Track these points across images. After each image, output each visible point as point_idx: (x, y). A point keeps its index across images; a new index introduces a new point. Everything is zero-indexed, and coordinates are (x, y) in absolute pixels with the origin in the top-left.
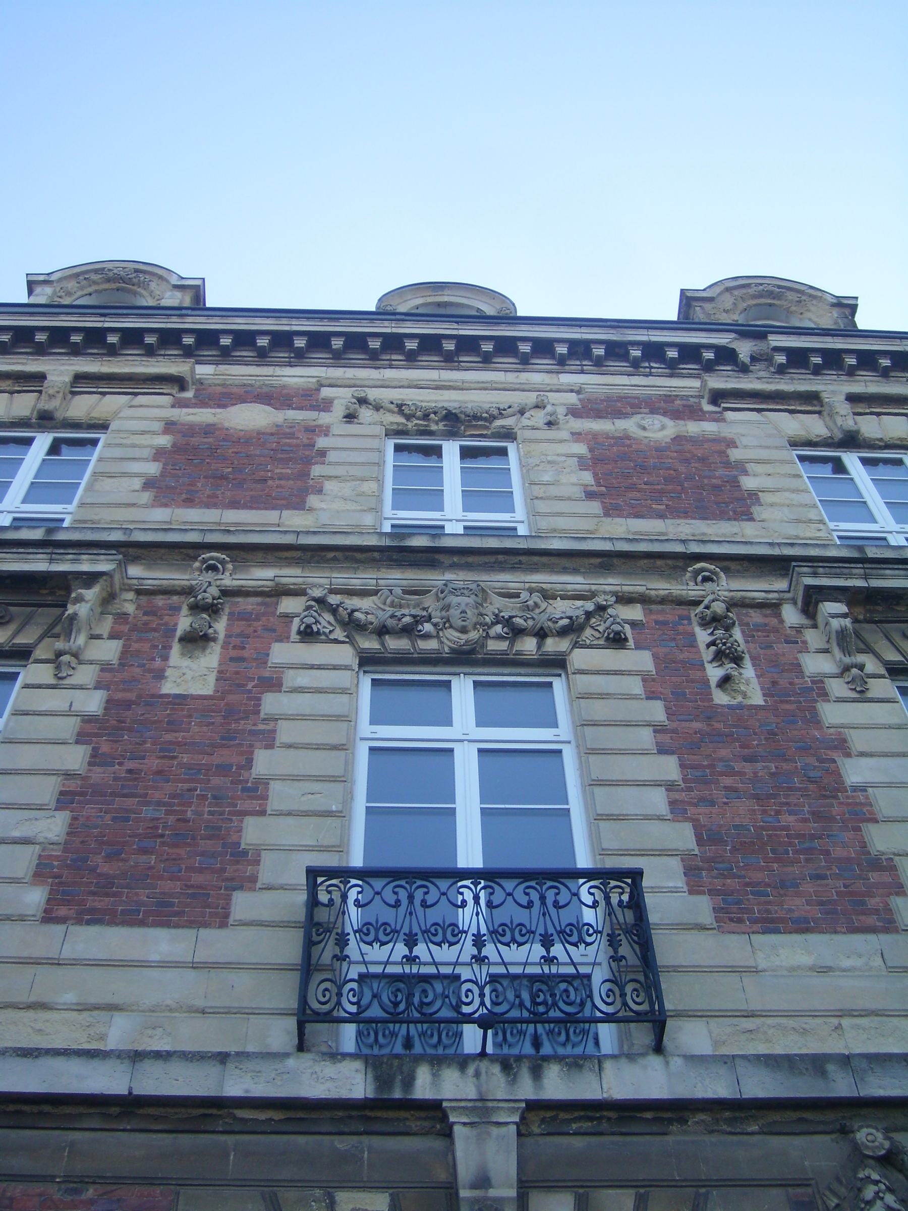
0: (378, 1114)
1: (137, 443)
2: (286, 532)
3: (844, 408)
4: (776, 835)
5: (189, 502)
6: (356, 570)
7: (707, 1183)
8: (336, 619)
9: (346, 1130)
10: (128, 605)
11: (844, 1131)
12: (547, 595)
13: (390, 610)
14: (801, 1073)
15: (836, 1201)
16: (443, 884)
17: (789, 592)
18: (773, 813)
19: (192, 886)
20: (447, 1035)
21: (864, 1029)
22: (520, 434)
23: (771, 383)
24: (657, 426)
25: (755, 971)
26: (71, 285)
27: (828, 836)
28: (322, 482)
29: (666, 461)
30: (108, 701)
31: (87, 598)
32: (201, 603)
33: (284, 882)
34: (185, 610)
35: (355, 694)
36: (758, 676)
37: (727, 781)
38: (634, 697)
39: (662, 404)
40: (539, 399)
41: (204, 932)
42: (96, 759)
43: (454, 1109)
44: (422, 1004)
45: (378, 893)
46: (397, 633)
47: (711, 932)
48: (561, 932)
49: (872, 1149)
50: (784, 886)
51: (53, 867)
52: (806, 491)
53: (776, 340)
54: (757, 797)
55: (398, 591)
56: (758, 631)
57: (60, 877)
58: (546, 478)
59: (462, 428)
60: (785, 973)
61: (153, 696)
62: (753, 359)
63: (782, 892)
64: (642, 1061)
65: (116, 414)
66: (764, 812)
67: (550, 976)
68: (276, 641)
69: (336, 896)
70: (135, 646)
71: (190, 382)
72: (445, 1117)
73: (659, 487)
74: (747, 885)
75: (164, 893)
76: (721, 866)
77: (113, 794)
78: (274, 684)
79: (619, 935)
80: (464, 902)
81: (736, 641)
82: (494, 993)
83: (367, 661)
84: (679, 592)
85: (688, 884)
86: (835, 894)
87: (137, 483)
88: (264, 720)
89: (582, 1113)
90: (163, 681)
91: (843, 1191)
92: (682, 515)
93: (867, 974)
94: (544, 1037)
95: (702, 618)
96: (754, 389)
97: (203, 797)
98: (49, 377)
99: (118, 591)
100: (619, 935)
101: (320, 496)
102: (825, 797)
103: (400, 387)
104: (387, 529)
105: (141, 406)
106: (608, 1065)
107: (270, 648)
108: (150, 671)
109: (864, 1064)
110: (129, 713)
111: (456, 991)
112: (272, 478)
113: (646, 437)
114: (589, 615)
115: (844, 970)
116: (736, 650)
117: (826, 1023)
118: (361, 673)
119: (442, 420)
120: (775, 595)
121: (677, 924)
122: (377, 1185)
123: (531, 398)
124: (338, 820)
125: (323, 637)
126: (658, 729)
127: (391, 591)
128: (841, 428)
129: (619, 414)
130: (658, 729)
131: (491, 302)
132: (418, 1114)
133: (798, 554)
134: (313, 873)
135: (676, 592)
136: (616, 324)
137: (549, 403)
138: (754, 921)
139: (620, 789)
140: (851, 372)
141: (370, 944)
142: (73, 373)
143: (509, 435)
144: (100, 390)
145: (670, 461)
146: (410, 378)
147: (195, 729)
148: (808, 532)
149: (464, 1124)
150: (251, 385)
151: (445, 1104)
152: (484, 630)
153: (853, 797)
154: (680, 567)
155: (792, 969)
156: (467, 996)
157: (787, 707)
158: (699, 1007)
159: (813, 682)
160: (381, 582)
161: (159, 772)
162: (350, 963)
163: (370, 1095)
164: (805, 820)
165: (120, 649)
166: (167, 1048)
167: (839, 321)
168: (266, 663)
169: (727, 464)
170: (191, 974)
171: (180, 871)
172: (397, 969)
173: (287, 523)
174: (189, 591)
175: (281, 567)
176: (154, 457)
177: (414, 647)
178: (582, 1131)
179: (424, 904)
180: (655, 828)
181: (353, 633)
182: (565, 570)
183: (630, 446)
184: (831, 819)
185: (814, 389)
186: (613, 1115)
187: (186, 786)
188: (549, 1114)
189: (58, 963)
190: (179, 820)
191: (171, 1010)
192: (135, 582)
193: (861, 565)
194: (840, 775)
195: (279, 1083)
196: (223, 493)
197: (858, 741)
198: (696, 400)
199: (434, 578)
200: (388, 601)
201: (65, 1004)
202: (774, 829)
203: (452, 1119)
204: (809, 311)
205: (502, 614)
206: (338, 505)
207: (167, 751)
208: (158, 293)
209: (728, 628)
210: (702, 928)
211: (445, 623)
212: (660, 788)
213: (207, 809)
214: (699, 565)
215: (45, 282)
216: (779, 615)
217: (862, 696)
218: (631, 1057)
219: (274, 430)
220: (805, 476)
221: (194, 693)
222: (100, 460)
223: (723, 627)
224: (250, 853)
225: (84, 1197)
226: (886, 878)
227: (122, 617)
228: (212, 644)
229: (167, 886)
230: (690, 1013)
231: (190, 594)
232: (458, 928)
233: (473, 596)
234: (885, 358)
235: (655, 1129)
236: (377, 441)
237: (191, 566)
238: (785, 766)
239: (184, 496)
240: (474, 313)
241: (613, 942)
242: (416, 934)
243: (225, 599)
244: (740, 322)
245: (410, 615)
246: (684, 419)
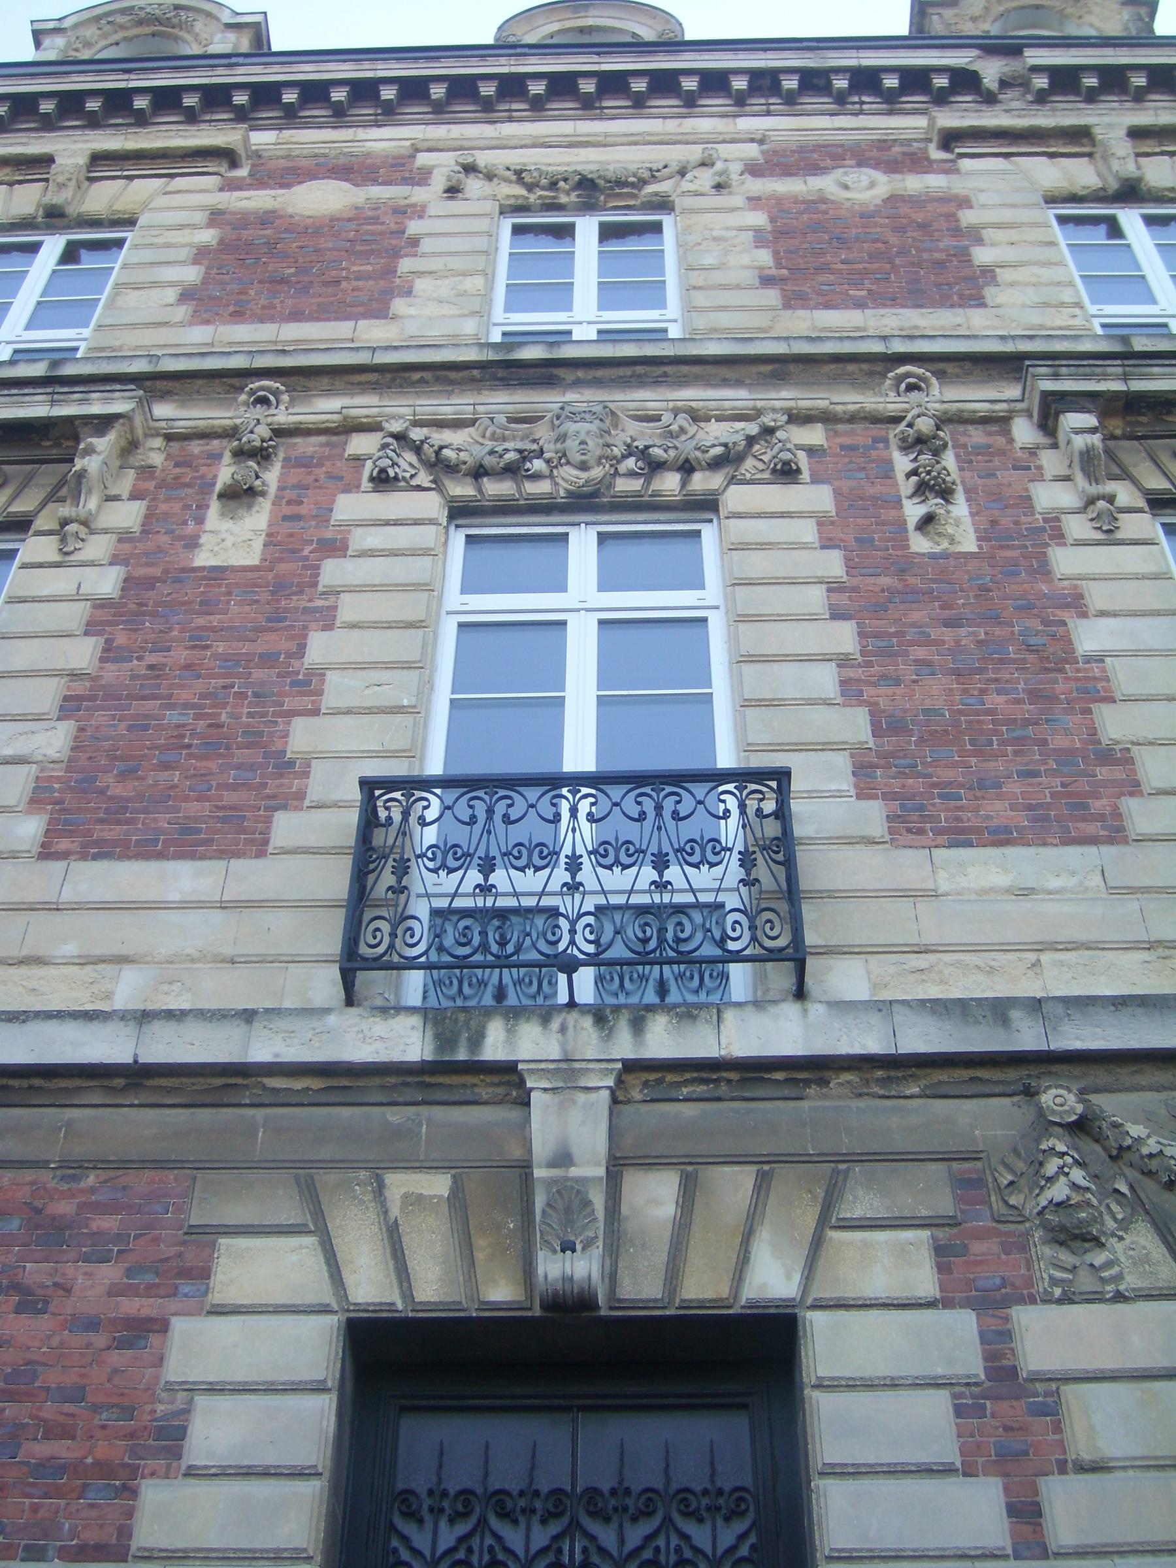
0: (441, 1079)
1: (173, 241)
2: (357, 349)
3: (1122, 147)
4: (978, 721)
5: (238, 316)
6: (449, 394)
7: (847, 1158)
8: (420, 460)
9: (401, 1099)
10: (155, 455)
11: (1030, 1093)
12: (697, 417)
13: (489, 444)
14: (977, 1022)
15: (1010, 1178)
16: (700, 790)
17: (1022, 401)
18: (976, 693)
19: (223, 808)
20: (711, 976)
21: (1069, 966)
22: (680, 203)
23: (1024, 116)
24: (865, 181)
25: (934, 895)
26: (90, 32)
27: (1047, 721)
28: (412, 281)
29: (874, 230)
30: (126, 580)
31: (99, 448)
32: (246, 447)
33: (339, 798)
34: (227, 457)
35: (440, 556)
36: (971, 514)
37: (920, 653)
38: (804, 546)
39: (875, 153)
40: (706, 155)
41: (236, 864)
42: (109, 654)
43: (531, 1071)
44: (678, 940)
45: (616, 804)
46: (498, 474)
47: (881, 846)
48: (764, 848)
49: (1061, 1114)
50: (985, 785)
51: (52, 790)
52: (1061, 264)
53: (1036, 57)
54: (957, 673)
55: (501, 419)
56: (978, 454)
57: (60, 802)
58: (709, 260)
59: (602, 198)
60: (973, 897)
61: (183, 570)
62: (1004, 84)
63: (978, 794)
64: (772, 1009)
65: (145, 206)
66: (965, 692)
67: (661, 907)
68: (344, 491)
69: (397, 816)
70: (163, 507)
71: (244, 156)
72: (522, 1082)
73: (861, 266)
74: (934, 785)
75: (188, 817)
76: (902, 762)
77: (130, 697)
78: (337, 548)
79: (754, 852)
80: (727, 811)
81: (945, 468)
82: (678, 928)
83: (459, 512)
84: (874, 406)
85: (856, 786)
86: (1048, 795)
87: (171, 295)
88: (324, 593)
89: (695, 1075)
90: (197, 551)
91: (1020, 1166)
92: (888, 303)
93: (1080, 896)
94: (672, 982)
95: (903, 440)
96: (1000, 127)
97: (242, 696)
98: (58, 160)
99: (141, 437)
100: (754, 852)
101: (408, 300)
102: (1048, 670)
103: (521, 147)
104: (496, 337)
105: (179, 192)
106: (729, 1015)
107: (334, 501)
108: (182, 538)
109: (1060, 1009)
110: (151, 593)
111: (720, 921)
112: (347, 278)
113: (849, 199)
114: (751, 440)
115: (1050, 893)
116: (944, 480)
117: (1020, 959)
118: (452, 528)
119: (574, 189)
120: (1004, 406)
121: (838, 838)
122: (435, 1164)
123: (695, 153)
124: (410, 718)
125: (403, 484)
126: (834, 587)
127: (492, 419)
128: (1116, 176)
129: (816, 169)
130: (834, 587)
131: (650, 22)
132: (489, 1079)
133: (1039, 349)
134: (368, 785)
135: (869, 407)
136: (815, 44)
137: (719, 158)
138: (938, 832)
139: (775, 666)
140: (1139, 96)
141: (610, 868)
142: (89, 152)
143: (664, 205)
144: (126, 173)
145: (879, 230)
146: (535, 133)
147: (234, 609)
148: (1059, 319)
149: (545, 1090)
150: (325, 156)
151: (520, 1066)
152: (611, 466)
153: (1085, 669)
154: (879, 373)
155: (984, 892)
156: (734, 930)
157: (1008, 553)
158: (857, 942)
159: (1045, 520)
160: (480, 408)
161: (188, 667)
162: (584, 893)
163: (428, 1057)
164: (1018, 701)
165: (143, 510)
166: (186, 1006)
167: (1130, 25)
168: (328, 520)
169: (957, 231)
170: (217, 916)
171: (209, 790)
172: (645, 899)
173: (364, 336)
174: (232, 433)
175: (352, 395)
176: (194, 259)
177: (520, 493)
178: (694, 1096)
179: (676, 817)
180: (819, 715)
181: (442, 477)
182: (725, 383)
183: (826, 212)
184: (1054, 699)
185: (1083, 123)
186: (734, 1076)
187: (221, 682)
188: (652, 1076)
189: (56, 908)
190: (210, 725)
191: (193, 961)
192: (163, 424)
193: (1119, 362)
194: (1070, 642)
195: (317, 1045)
196: (282, 302)
197: (1098, 596)
198: (921, 145)
199: (548, 400)
200: (488, 433)
201: (64, 957)
202: (977, 713)
203: (529, 1084)
204: (1090, 12)
205: (635, 444)
206: (432, 309)
207: (198, 640)
208: (205, 36)
209: (937, 453)
210: (871, 841)
211: (560, 458)
212: (828, 664)
213: (246, 710)
214: (902, 370)
215: (57, 31)
216: (1007, 433)
217: (1109, 536)
218: (758, 1004)
219: (351, 214)
220: (1063, 243)
221: (236, 564)
222: (125, 266)
223: (930, 450)
224: (298, 762)
225: (83, 1185)
226: (1118, 773)
227: (147, 471)
228: (261, 499)
229: (194, 808)
230: (845, 949)
231: (233, 436)
232: (719, 842)
233: (597, 422)
234: (739, 77)
235: (786, 1092)
236: (486, 221)
237: (235, 399)
238: (997, 631)
239: (231, 308)
240: (629, 39)
241: (747, 860)
242: (494, 858)
243: (279, 440)
244: (992, 34)
245: (515, 450)
246: (901, 172)
